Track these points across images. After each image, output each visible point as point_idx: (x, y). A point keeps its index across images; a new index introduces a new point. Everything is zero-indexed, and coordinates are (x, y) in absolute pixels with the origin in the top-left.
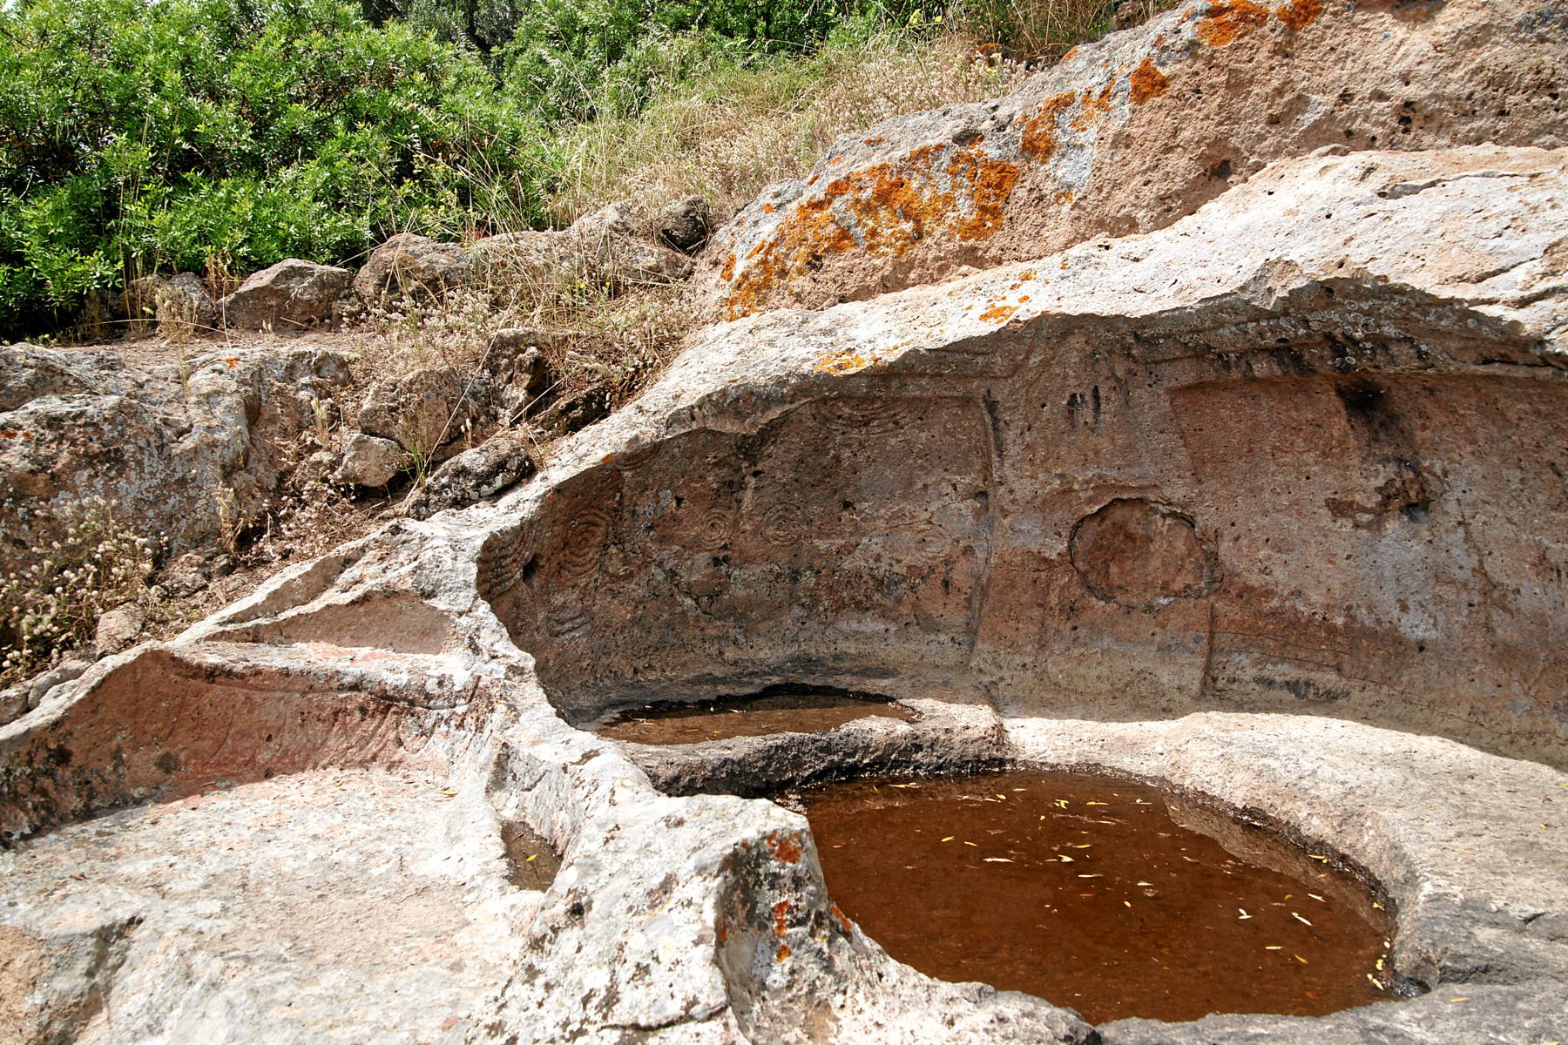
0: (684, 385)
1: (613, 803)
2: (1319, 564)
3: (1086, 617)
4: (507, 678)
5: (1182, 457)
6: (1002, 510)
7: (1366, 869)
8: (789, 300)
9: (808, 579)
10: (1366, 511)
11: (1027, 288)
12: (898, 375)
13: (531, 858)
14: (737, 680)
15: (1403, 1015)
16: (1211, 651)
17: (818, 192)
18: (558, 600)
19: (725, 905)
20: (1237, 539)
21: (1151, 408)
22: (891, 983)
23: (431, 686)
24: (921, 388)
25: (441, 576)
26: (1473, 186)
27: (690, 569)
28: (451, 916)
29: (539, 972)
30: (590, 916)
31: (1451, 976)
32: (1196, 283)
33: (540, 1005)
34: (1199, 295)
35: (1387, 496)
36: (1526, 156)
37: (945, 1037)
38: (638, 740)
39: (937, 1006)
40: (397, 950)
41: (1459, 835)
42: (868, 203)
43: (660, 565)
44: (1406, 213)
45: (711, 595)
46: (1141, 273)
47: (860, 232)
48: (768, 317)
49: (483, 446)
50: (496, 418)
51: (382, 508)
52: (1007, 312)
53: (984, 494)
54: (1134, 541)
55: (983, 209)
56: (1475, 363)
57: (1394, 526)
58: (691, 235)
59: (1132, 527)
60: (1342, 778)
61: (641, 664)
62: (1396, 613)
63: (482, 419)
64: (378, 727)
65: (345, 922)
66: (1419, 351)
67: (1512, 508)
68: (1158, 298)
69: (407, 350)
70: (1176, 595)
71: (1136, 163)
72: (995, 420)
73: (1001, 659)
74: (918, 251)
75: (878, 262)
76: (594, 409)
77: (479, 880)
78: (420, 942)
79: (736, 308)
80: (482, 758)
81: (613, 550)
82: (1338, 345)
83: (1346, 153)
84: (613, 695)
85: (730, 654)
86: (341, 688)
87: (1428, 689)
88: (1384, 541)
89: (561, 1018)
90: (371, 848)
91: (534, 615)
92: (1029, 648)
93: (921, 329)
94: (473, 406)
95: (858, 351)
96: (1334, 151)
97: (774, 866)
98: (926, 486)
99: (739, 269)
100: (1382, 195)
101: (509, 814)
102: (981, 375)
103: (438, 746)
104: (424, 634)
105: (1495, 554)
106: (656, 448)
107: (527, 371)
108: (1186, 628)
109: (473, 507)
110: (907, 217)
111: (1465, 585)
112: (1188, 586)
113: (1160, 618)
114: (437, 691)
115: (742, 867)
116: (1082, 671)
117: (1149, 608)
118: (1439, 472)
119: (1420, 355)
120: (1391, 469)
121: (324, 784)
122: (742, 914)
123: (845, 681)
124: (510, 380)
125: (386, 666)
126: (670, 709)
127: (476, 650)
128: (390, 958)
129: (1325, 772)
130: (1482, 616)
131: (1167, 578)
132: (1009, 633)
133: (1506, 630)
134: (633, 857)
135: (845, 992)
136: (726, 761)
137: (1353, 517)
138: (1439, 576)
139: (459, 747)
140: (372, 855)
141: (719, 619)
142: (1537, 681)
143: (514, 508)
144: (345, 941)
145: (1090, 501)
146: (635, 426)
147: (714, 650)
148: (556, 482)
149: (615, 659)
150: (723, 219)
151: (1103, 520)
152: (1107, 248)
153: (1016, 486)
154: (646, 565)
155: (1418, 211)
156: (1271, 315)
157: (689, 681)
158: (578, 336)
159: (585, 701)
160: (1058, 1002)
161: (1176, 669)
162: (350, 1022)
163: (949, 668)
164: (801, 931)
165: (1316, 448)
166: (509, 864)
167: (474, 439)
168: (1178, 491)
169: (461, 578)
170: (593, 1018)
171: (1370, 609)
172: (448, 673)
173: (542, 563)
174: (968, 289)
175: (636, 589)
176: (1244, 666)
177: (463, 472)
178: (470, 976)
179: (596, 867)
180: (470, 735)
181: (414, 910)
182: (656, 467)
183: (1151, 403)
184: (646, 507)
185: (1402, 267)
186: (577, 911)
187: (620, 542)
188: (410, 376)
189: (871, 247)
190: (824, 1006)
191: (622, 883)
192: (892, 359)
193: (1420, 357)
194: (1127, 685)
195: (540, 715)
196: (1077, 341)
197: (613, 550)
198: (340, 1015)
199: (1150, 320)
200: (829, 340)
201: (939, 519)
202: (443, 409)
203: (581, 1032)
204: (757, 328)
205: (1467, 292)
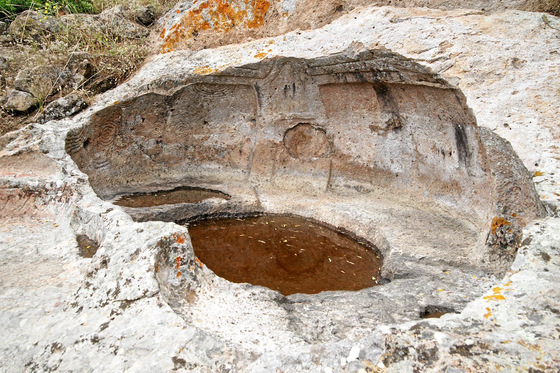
0: (145, 77)
1: (118, 225)
2: (366, 147)
3: (289, 164)
4: (78, 183)
5: (323, 109)
6: (261, 126)
7: (375, 246)
8: (185, 46)
9: (191, 149)
10: (381, 129)
11: (271, 47)
12: (224, 76)
13: (87, 246)
14: (165, 185)
15: (382, 289)
16: (330, 176)
17: (196, 6)
18: (97, 155)
19: (158, 257)
20: (340, 138)
21: (313, 92)
22: (216, 283)
23: (48, 186)
24: (233, 81)
25: (50, 145)
26: (419, 20)
27: (148, 145)
28: (57, 268)
29: (91, 284)
30: (109, 264)
31: (397, 277)
32: (329, 48)
33: (91, 295)
34: (330, 52)
35: (389, 124)
36: (436, 12)
37: (234, 300)
38: (128, 206)
39: (232, 290)
40: (36, 281)
41: (404, 234)
42: (215, 12)
43: (136, 143)
44: (398, 28)
45: (156, 154)
46: (311, 44)
47: (212, 23)
48: (177, 53)
49: (67, 96)
50: (72, 86)
51: (25, 119)
52: (264, 55)
53: (254, 120)
54: (305, 138)
55: (257, 17)
56: (417, 81)
57: (390, 135)
58: (148, 20)
59: (305, 133)
60: (370, 217)
61: (129, 179)
62: (390, 164)
63: (66, 86)
64: (26, 201)
65: (15, 272)
66: (400, 76)
67: (426, 130)
69: (33, 58)
70: (319, 156)
72: (259, 94)
73: (259, 178)
74: (232, 31)
75: (218, 34)
76: (110, 85)
77: (68, 255)
78: (46, 278)
79: (166, 49)
80: (68, 212)
81: (118, 137)
82: (375, 72)
83: (381, 6)
84: (119, 190)
85: (163, 176)
86: (10, 187)
87: (399, 189)
88: (387, 140)
89: (99, 299)
90: (25, 246)
91: (88, 160)
92: (269, 174)
93: (233, 59)
94: (63, 81)
95: (210, 67)
96: (377, 5)
97: (175, 245)
98: (234, 117)
99: (166, 34)
100: (391, 21)
101: (79, 232)
102: (254, 77)
103: (51, 208)
104: (44, 167)
105: (421, 145)
106: (135, 100)
107: (84, 68)
108: (322, 168)
109: (63, 120)
110: (229, 18)
111: (411, 155)
112: (323, 154)
113: (314, 165)
114: (50, 188)
115: (164, 246)
116: (287, 182)
117: (310, 161)
118: (405, 117)
119: (400, 77)
120: (391, 114)
121: (5, 223)
122: (164, 261)
123: (204, 186)
124: (77, 72)
125: (30, 178)
126: (140, 195)
127: (65, 173)
128: (33, 284)
129: (365, 215)
130: (416, 164)
131: (317, 151)
132: (262, 169)
133: (423, 170)
134: (125, 243)
135: (200, 287)
136: (161, 213)
137: (378, 131)
138: (404, 152)
139: (59, 208)
140: (25, 248)
141: (159, 163)
142: (431, 186)
143: (80, 120)
144: (15, 279)
145: (291, 123)
146: (126, 91)
147: (157, 174)
148: (96, 111)
149: (120, 178)
150: (160, 14)
151: (295, 130)
154: (131, 143)
155: (403, 28)
156: (354, 61)
157: (147, 185)
158: (104, 56)
159: (108, 192)
160: (275, 289)
161: (318, 182)
162: (18, 306)
163: (241, 181)
164: (185, 267)
166: (80, 249)
167: (63, 94)
168: (321, 121)
169: (59, 146)
170: (111, 299)
171: (382, 162)
172: (54, 182)
173: (91, 141)
174: (251, 46)
175: (127, 152)
176: (340, 181)
177: (58, 106)
178: (65, 288)
179: (111, 247)
180: (64, 204)
181: (43, 267)
182: (135, 106)
183: (313, 89)
184: (131, 122)
185: (396, 47)
186: (105, 263)
187: (121, 134)
188: (35, 68)
189: (216, 29)
190: (194, 292)
191: (121, 252)
192: (222, 70)
193: (400, 78)
194: (302, 187)
195: (91, 196)
196: (288, 67)
197: (118, 137)
198: (14, 304)
199: (313, 61)
200: (199, 62)
202: (50, 82)
203: (107, 304)
204: (173, 56)
205: (415, 57)
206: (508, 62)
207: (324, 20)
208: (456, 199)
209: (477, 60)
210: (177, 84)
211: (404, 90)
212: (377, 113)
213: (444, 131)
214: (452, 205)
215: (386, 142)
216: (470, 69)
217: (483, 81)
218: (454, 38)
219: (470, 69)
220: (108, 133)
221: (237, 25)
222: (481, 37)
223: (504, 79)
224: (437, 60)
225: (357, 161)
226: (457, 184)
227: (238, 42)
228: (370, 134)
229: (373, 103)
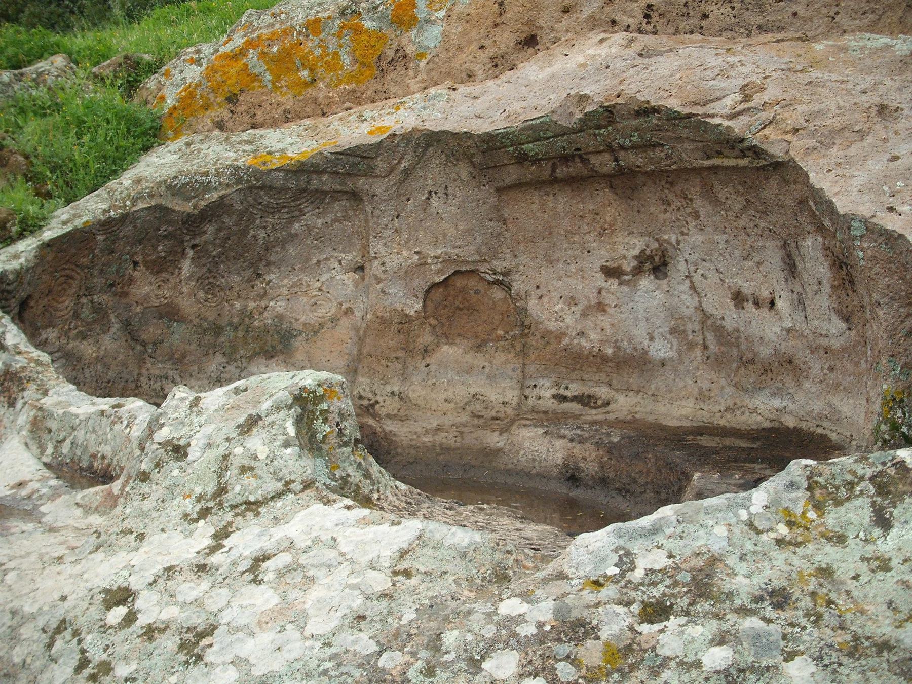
6: (376, 278)
20: (541, 298)
32: (520, 111)
46: (480, 106)
57: (646, 282)
62: (646, 342)
67: (719, 262)
68: (493, 122)
71: (474, 33)
88: (639, 293)
98: (319, 262)
100: (641, 55)
105: (709, 295)
141: (161, 362)
145: (438, 272)
152: (454, 89)
153: (386, 260)
155: (665, 66)
165: (595, 230)
173: (32, 304)
182: (122, 234)
194: (466, 404)
201: (328, 287)
205: (699, 110)
206: (871, 110)
207: (499, 64)
208: (790, 391)
209: (816, 109)
210: (207, 188)
211: (672, 184)
212: (615, 239)
213: (757, 259)
214: (784, 404)
215: (637, 299)
216: (805, 124)
217: (834, 144)
218: (765, 78)
219: (805, 124)
220: (64, 289)
221: (322, 79)
222: (814, 74)
223: (870, 139)
224: (740, 113)
225: (579, 344)
226: (790, 362)
227: (324, 114)
228: (604, 284)
229: (608, 219)
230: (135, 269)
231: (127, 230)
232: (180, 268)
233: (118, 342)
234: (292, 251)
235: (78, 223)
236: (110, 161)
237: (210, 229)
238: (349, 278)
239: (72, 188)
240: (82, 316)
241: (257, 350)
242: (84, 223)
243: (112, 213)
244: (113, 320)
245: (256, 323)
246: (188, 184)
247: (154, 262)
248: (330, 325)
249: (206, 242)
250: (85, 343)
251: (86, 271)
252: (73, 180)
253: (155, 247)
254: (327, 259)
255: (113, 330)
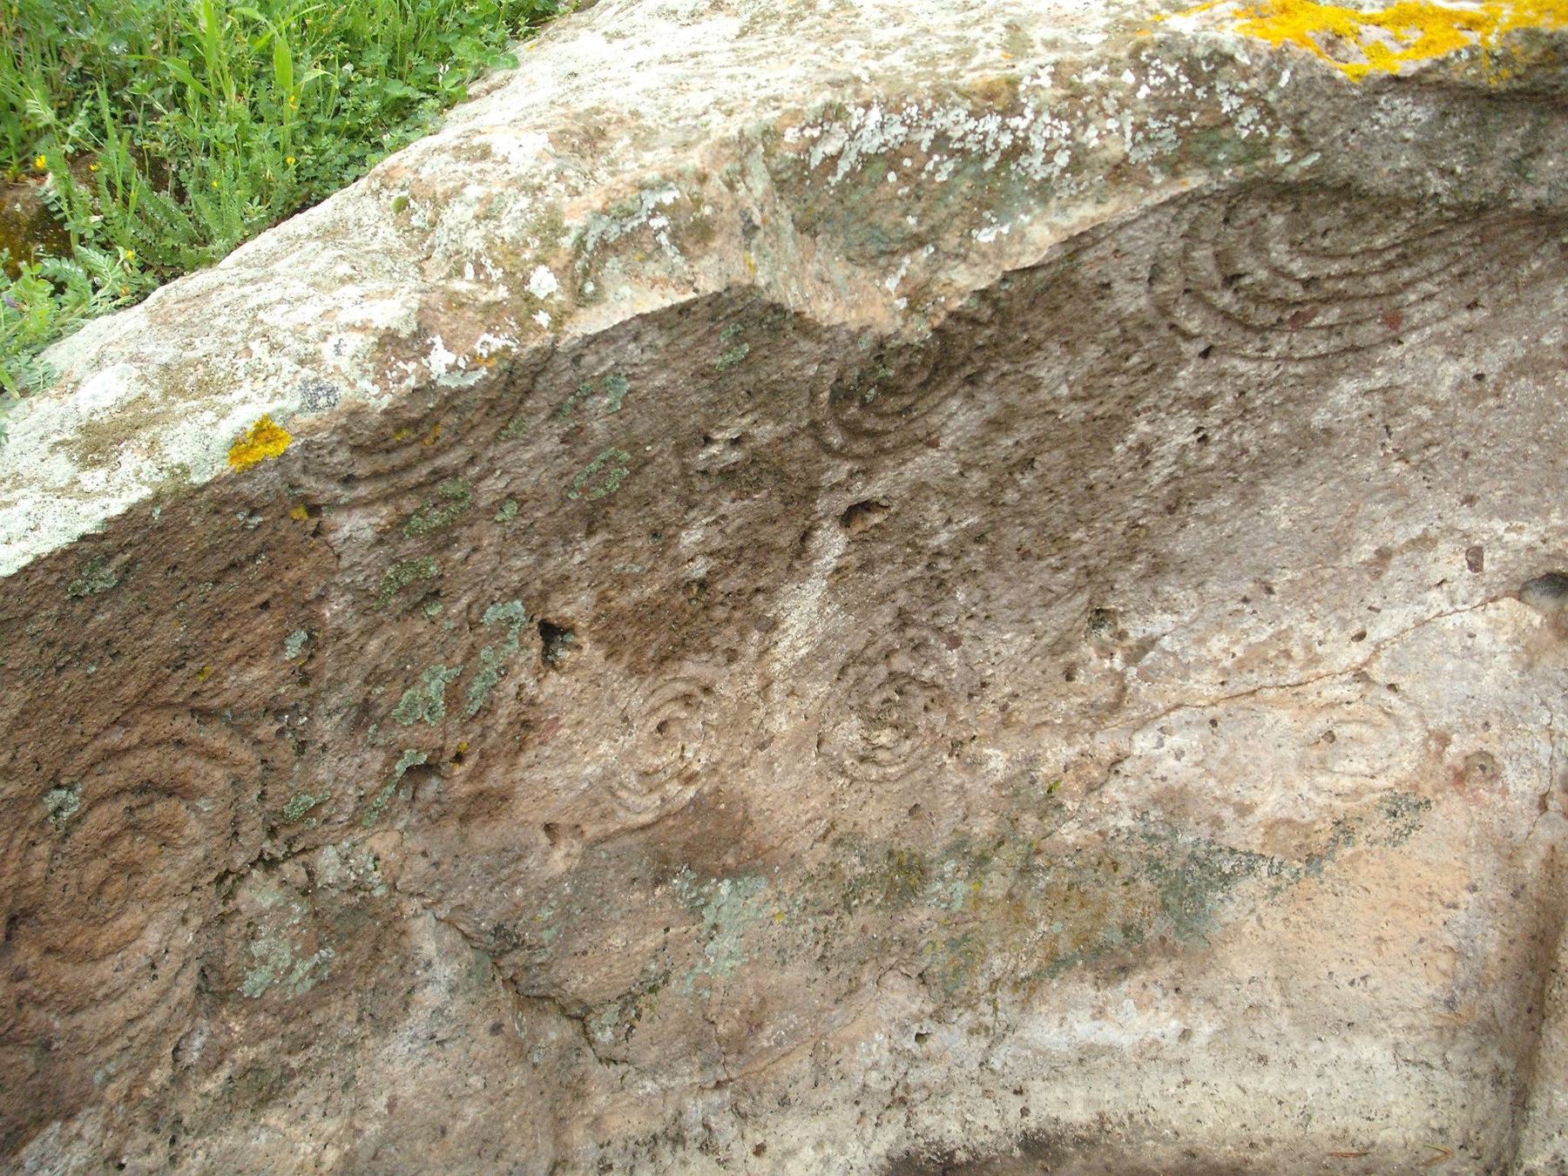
98: (1384, 555)
141: (653, 1071)
182: (495, 485)
210: (996, 181)
220: (132, 869)
230: (549, 661)
231: (531, 459)
232: (773, 625)
233: (454, 1051)
234: (1283, 507)
235: (198, 445)
236: (377, 57)
237: (957, 418)
238: (1496, 626)
239: (180, 194)
240: (255, 981)
241: (1065, 946)
242: (238, 445)
243: (440, 360)
244: (429, 948)
245: (1070, 833)
246: (891, 158)
247: (646, 616)
248: (1381, 827)
249: (920, 488)
250: (275, 1117)
251: (266, 730)
252: (184, 148)
253: (661, 536)
254: (1424, 542)
255: (431, 996)
